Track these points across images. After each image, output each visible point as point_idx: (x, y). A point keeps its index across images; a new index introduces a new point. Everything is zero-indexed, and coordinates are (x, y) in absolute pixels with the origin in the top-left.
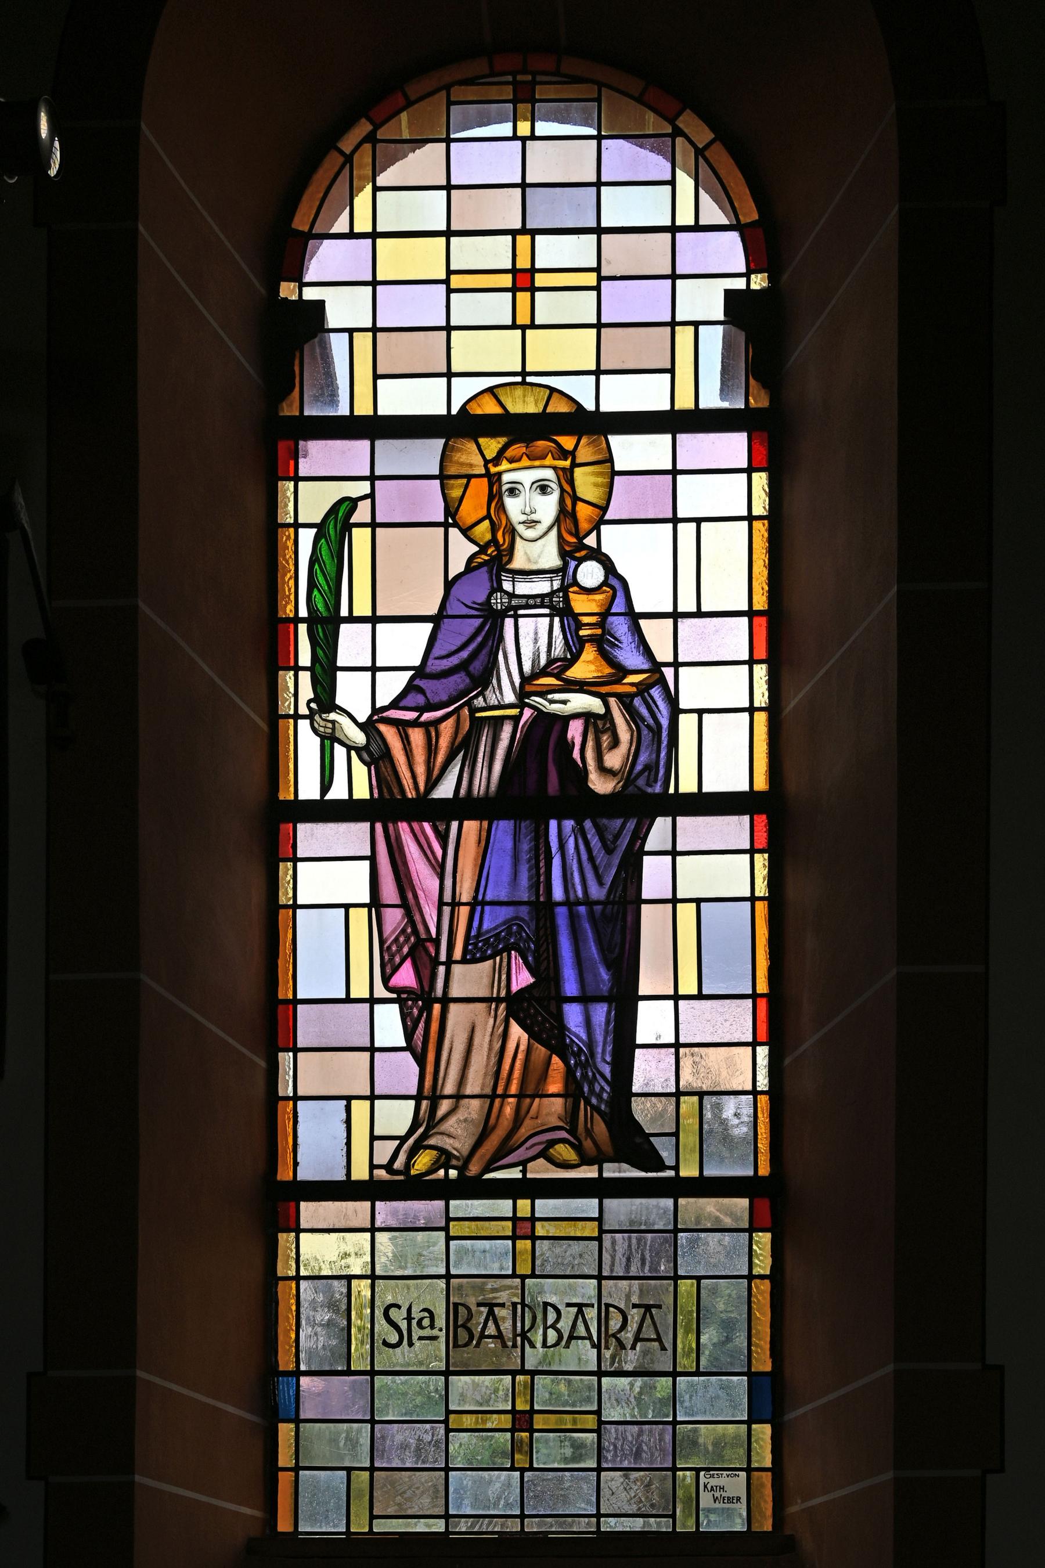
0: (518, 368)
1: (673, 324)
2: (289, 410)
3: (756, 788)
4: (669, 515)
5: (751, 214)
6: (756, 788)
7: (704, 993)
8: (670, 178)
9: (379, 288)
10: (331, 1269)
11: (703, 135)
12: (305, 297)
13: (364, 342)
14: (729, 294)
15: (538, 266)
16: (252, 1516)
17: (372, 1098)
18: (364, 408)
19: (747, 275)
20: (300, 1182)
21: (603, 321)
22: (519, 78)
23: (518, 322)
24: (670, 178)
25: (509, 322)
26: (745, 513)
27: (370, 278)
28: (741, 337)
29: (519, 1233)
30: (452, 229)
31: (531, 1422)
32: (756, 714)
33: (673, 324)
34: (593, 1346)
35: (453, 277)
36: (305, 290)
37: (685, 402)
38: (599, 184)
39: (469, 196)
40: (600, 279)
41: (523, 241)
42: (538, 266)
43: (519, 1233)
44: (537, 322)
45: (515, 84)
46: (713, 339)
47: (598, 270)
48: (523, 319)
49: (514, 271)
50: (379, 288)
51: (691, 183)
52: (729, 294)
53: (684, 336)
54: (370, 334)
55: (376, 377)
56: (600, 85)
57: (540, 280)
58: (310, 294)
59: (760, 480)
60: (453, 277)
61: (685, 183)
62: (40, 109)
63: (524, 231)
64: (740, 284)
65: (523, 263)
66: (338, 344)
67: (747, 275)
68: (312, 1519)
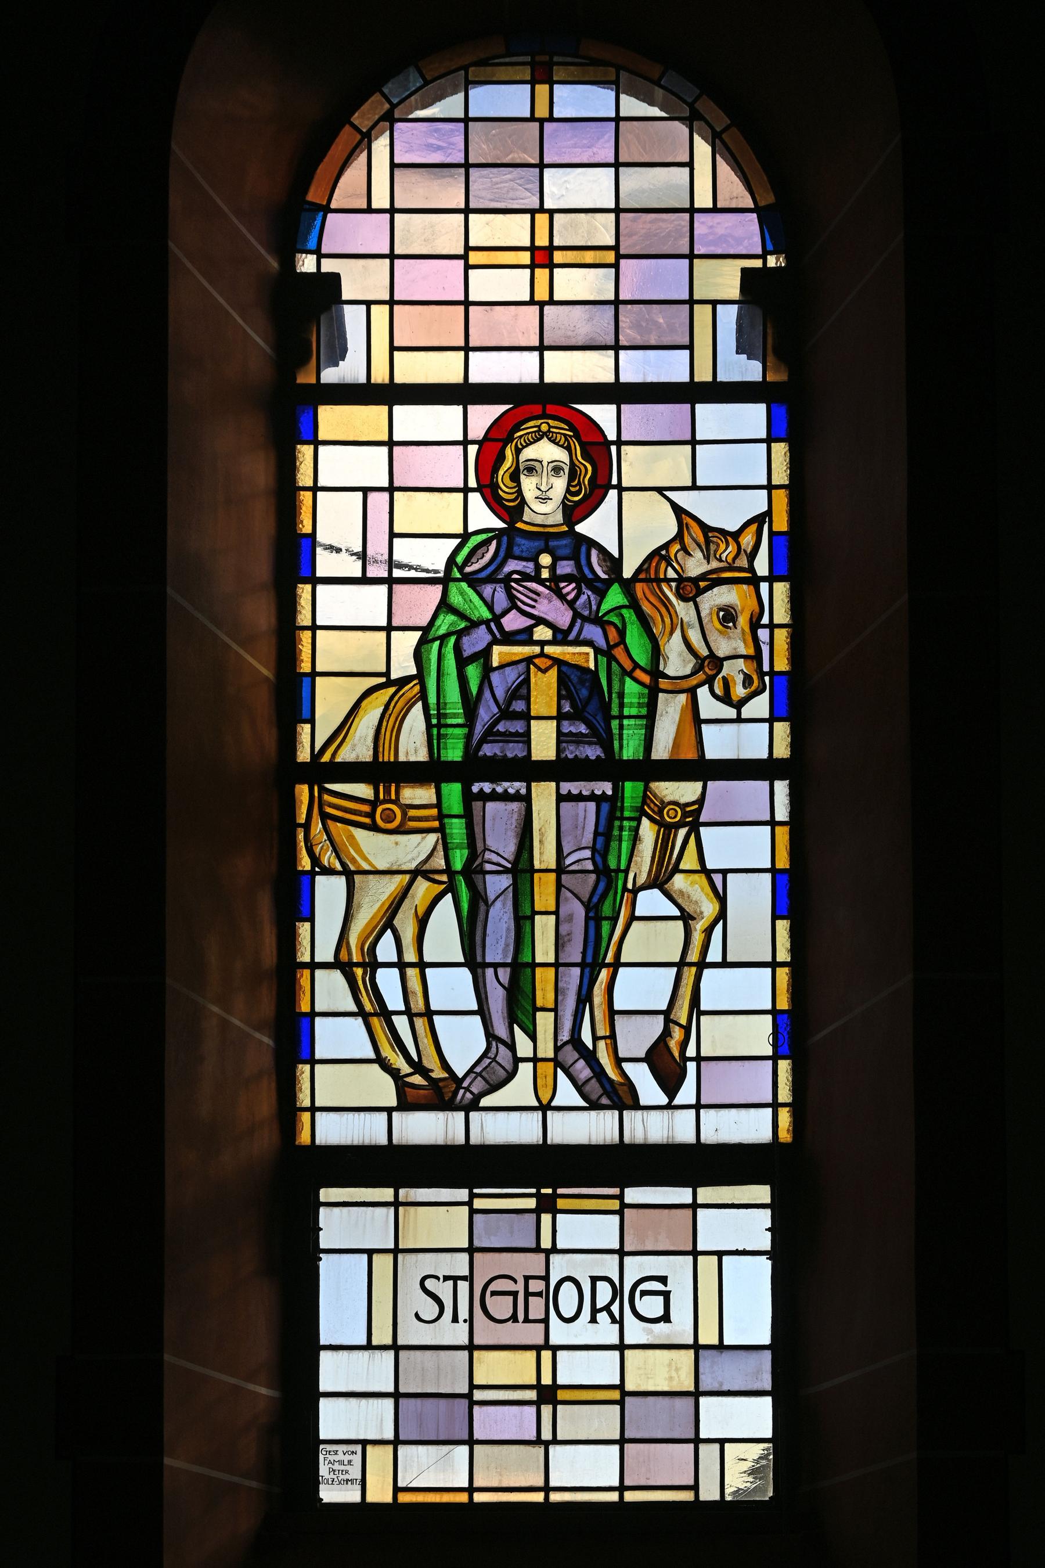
0: (540, 1482)
1: (691, 302)
2: (307, 378)
3: (768, 1200)
4: (688, 437)
5: (768, 199)
6: (768, 1200)
7: (728, 960)
8: (688, 160)
10: (345, 1495)
11: (721, 121)
12: (324, 270)
13: (380, 314)
14: (745, 271)
18: (380, 375)
21: (622, 114)
22: (538, 58)
23: (537, 115)
24: (688, 160)
25: (527, 298)
27: (396, 449)
28: (758, 313)
32: (776, 631)
33: (691, 302)
34: (614, 1320)
35: (471, 254)
36: (324, 262)
37: (704, 375)
39: (505, 1468)
41: (542, 112)
44: (559, 1438)
45: (533, 65)
46: (728, 315)
47: (616, 248)
48: (542, 219)
49: (533, 249)
51: (709, 149)
52: (745, 271)
53: (703, 313)
54: (387, 261)
55: (393, 349)
56: (618, 68)
57: (561, 1395)
58: (328, 266)
59: (780, 449)
60: (471, 254)
61: (703, 149)
63: (548, 1253)
64: (758, 263)
65: (542, 241)
66: (353, 318)
67: (763, 257)
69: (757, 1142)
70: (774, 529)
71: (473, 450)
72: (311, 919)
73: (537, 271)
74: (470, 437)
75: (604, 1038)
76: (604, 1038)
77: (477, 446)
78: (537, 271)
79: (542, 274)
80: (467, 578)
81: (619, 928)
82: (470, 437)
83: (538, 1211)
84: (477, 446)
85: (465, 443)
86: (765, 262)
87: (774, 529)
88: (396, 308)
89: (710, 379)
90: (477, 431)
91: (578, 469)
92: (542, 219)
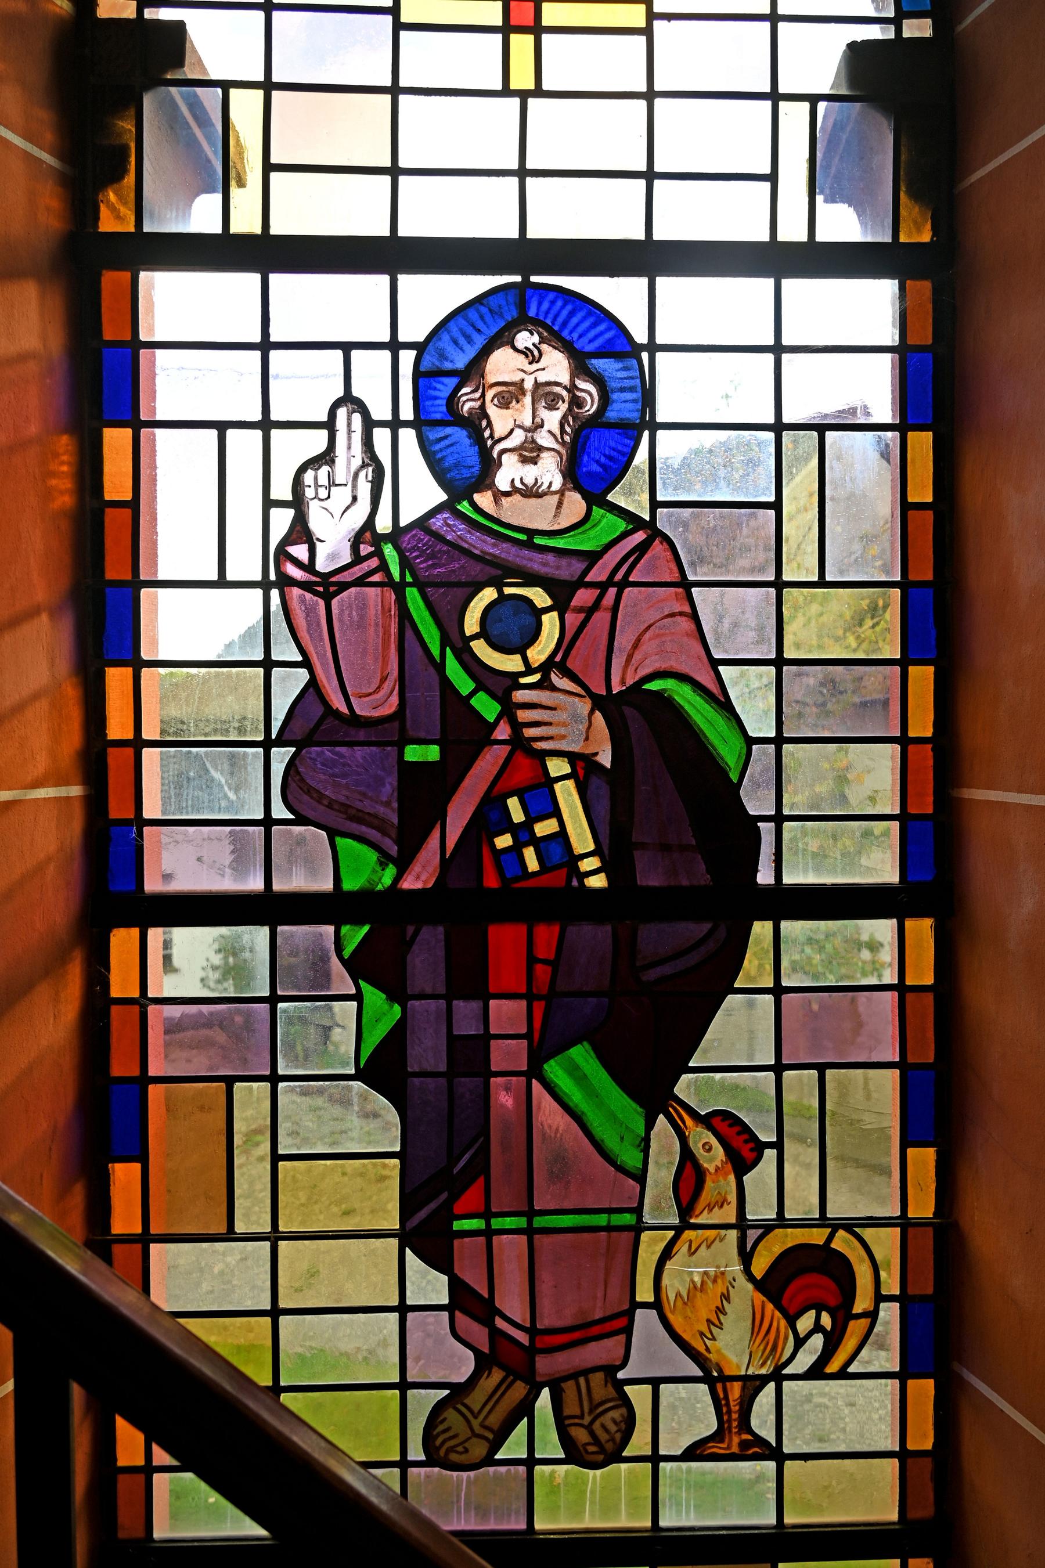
9: (514, 165)
15: (498, 38)
16: (973, 1373)
17: (268, 86)
19: (896, 22)
20: (262, 923)
23: (514, 85)
26: (402, 179)
29: (529, 21)
30: (528, 237)
31: (522, 30)
38: (779, 662)
40: (524, 96)
42: (498, 38)
43: (529, 21)
48: (522, 79)
50: (514, 165)
62: (473, 379)
64: (874, 33)
68: (553, 1512)
69: (200, 271)
70: (137, 1167)
71: (407, 358)
72: (142, 1156)
73: (514, 38)
74: (402, 338)
75: (545, 962)
76: (545, 962)
77: (413, 353)
78: (514, 38)
79: (522, 44)
80: (764, 1380)
81: (417, 608)
82: (402, 338)
83: (507, 29)
84: (413, 353)
85: (394, 346)
86: (899, 31)
87: (137, 1167)
88: (260, 77)
89: (803, 237)
90: (413, 330)
91: (583, 394)
92: (522, 79)
